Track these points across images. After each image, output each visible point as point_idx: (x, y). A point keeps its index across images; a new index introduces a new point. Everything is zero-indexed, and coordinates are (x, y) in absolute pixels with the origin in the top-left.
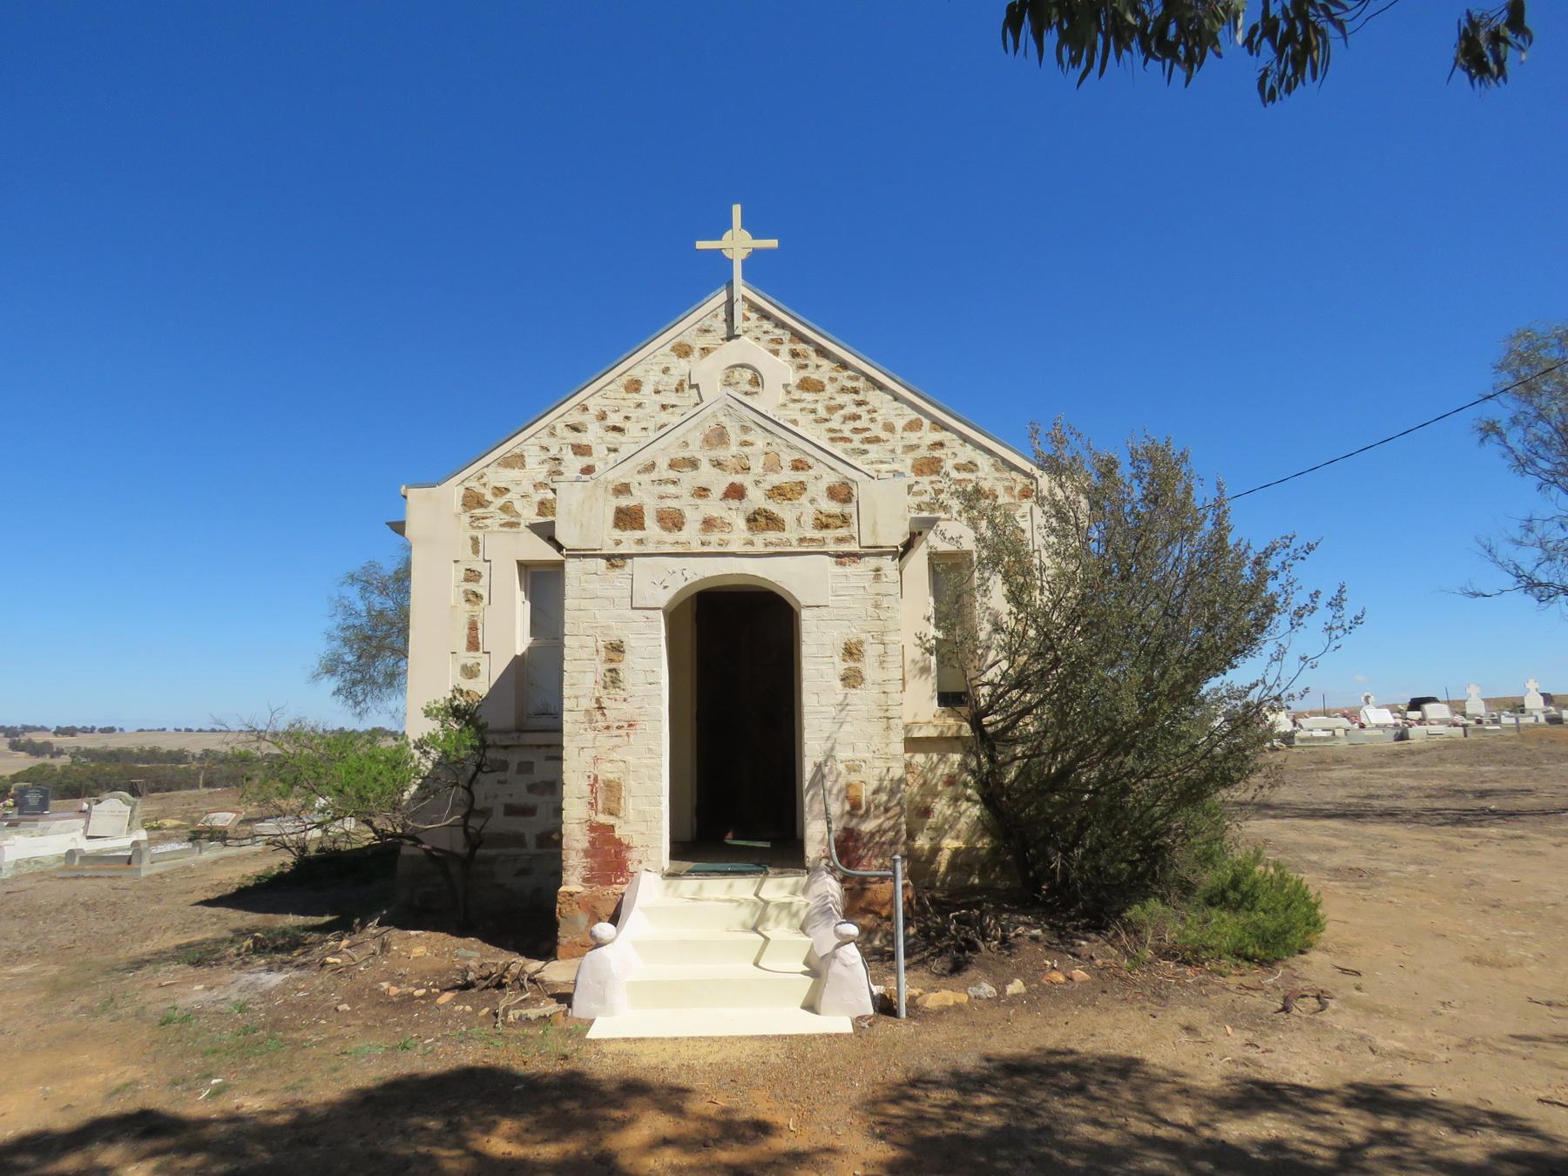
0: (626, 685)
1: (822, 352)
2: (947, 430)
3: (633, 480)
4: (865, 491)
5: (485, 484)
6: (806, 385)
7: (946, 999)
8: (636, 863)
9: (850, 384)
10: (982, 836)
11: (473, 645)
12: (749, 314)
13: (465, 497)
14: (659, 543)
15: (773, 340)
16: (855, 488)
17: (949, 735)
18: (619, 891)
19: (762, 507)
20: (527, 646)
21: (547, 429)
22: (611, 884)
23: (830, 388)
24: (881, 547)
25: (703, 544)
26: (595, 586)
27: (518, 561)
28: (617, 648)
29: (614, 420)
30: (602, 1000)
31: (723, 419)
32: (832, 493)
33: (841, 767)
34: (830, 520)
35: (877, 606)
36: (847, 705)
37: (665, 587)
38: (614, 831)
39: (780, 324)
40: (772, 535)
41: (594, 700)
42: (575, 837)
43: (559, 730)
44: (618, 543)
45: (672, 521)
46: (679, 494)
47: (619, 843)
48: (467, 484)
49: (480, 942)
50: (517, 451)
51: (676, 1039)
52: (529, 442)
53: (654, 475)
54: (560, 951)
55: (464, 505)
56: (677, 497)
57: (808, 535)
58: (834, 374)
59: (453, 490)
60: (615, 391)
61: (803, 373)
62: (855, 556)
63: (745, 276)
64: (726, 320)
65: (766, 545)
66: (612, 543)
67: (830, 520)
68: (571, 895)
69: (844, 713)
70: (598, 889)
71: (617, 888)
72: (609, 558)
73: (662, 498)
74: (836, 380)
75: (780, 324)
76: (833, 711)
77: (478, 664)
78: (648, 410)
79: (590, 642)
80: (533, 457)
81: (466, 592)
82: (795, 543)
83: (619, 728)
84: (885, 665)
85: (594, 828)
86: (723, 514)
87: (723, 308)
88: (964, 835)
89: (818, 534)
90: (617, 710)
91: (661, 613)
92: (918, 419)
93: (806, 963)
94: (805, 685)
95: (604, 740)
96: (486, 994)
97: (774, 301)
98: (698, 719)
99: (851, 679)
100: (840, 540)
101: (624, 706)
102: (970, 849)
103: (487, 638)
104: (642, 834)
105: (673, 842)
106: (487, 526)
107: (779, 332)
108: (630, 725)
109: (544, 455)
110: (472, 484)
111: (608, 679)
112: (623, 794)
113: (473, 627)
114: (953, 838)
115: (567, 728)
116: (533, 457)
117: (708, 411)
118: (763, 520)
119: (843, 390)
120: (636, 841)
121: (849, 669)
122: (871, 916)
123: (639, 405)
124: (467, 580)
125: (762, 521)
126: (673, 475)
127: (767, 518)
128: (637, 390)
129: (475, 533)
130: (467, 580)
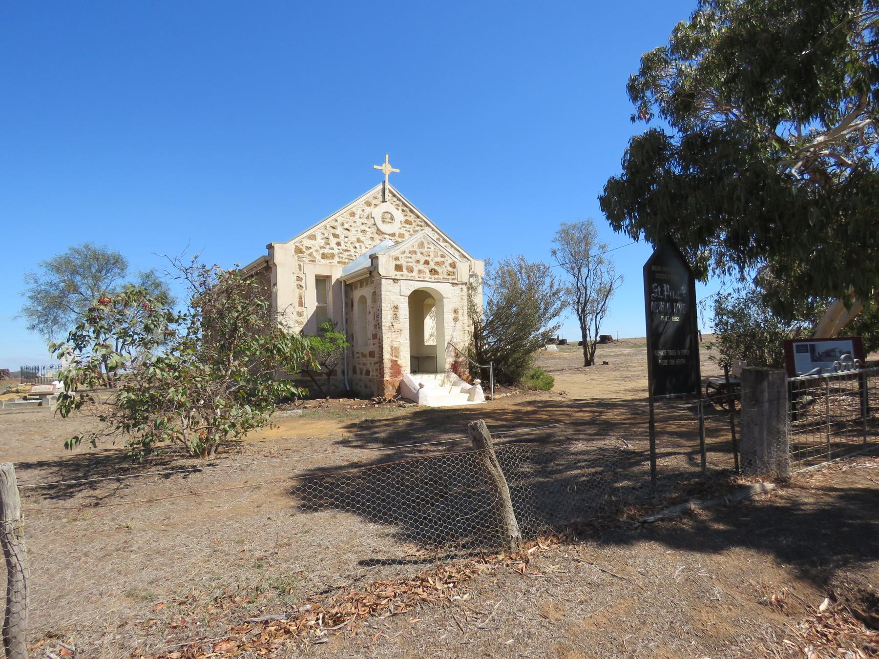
1: (411, 211)
3: (400, 256)
4: (458, 265)
6: (407, 222)
9: (420, 224)
11: (301, 304)
23: (414, 224)
28: (396, 307)
29: (346, 226)
39: (399, 200)
40: (436, 276)
42: (387, 364)
45: (411, 270)
47: (399, 365)
52: (317, 230)
53: (405, 255)
59: (291, 246)
61: (406, 218)
72: (394, 280)
75: (399, 200)
78: (358, 224)
79: (389, 305)
80: (319, 236)
85: (392, 361)
90: (397, 326)
99: (456, 319)
100: (453, 279)
107: (398, 202)
109: (323, 237)
110: (298, 244)
113: (300, 298)
115: (384, 331)
116: (319, 236)
119: (418, 225)
120: (403, 365)
123: (355, 222)
124: (297, 280)
126: (410, 255)
128: (354, 216)
129: (300, 263)
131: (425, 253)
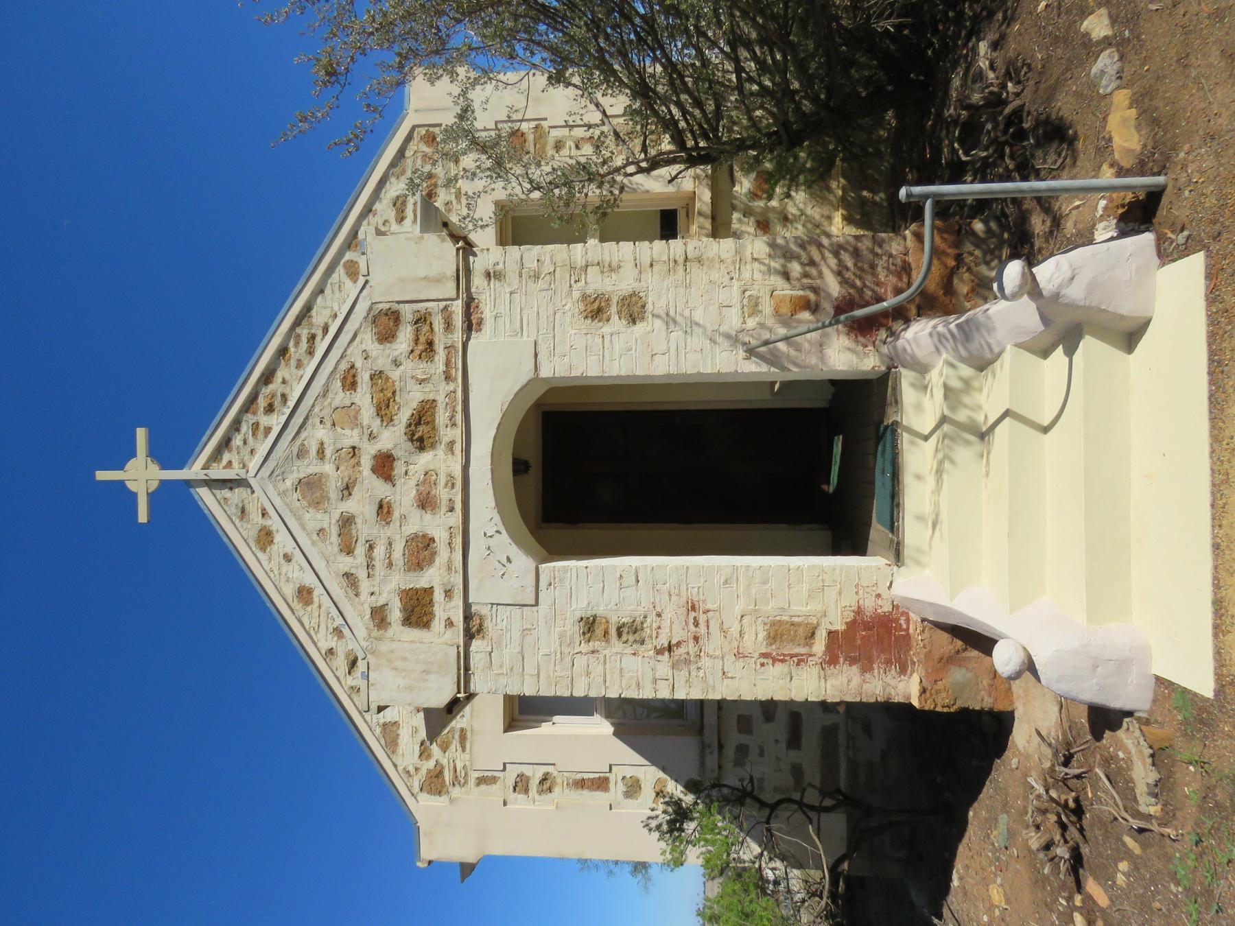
0: (640, 612)
1: (267, 378)
2: (356, 233)
3: (367, 602)
4: (385, 291)
5: (417, 769)
7: (1124, 121)
8: (880, 602)
9: (304, 345)
10: (828, 189)
11: (601, 784)
12: (224, 462)
13: (430, 792)
14: (449, 569)
15: (254, 434)
16: (381, 306)
17: (710, 227)
18: (919, 625)
19: (403, 430)
20: (604, 720)
21: (353, 696)
22: (908, 635)
24: (458, 270)
25: (452, 510)
26: (507, 654)
27: (505, 731)
28: (590, 626)
30: (1122, 664)
31: (288, 483)
32: (386, 337)
33: (751, 323)
34: (422, 339)
35: (536, 276)
36: (668, 315)
37: (509, 560)
38: (836, 632)
39: (236, 425)
40: (442, 417)
41: (660, 657)
43: (701, 703)
44: (450, 623)
46: (386, 541)
47: (852, 625)
48: (416, 789)
49: (976, 805)
50: (378, 731)
51: (1216, 547)
53: (362, 574)
54: (1000, 706)
55: (440, 793)
56: (390, 544)
57: (442, 368)
58: (293, 363)
59: (423, 807)
60: (311, 617)
62: (470, 305)
63: (180, 467)
64: (231, 489)
65: (454, 425)
66: (449, 633)
67: (422, 339)
68: (924, 691)
69: (679, 319)
70: (916, 652)
71: (914, 629)
72: (469, 635)
73: (390, 565)
74: (299, 360)
75: (236, 425)
76: (677, 335)
77: (624, 778)
79: (581, 662)
81: (541, 792)
82: (451, 387)
83: (696, 624)
84: (614, 264)
85: (831, 658)
86: (413, 482)
87: (217, 492)
88: (826, 210)
89: (441, 356)
90: (673, 627)
91: (544, 567)
92: (345, 266)
93: (1045, 353)
94: (640, 372)
95: (714, 644)
96: (1094, 833)
97: (208, 432)
98: (688, 521)
99: (633, 309)
100: (448, 326)
101: (667, 616)
102: (844, 202)
103: (593, 766)
104: (840, 593)
105: (836, 550)
106: (465, 767)
107: (244, 428)
108: (693, 608)
111: (631, 638)
112: (786, 618)
113: (581, 784)
114: (831, 224)
115: (696, 694)
117: (278, 502)
118: (421, 428)
120: (850, 601)
121: (619, 313)
122: (956, 281)
124: (526, 791)
125: (422, 430)
126: (360, 550)
127: (418, 423)
128: (310, 591)
129: (472, 781)
130: (526, 791)
131: (345, 472)
